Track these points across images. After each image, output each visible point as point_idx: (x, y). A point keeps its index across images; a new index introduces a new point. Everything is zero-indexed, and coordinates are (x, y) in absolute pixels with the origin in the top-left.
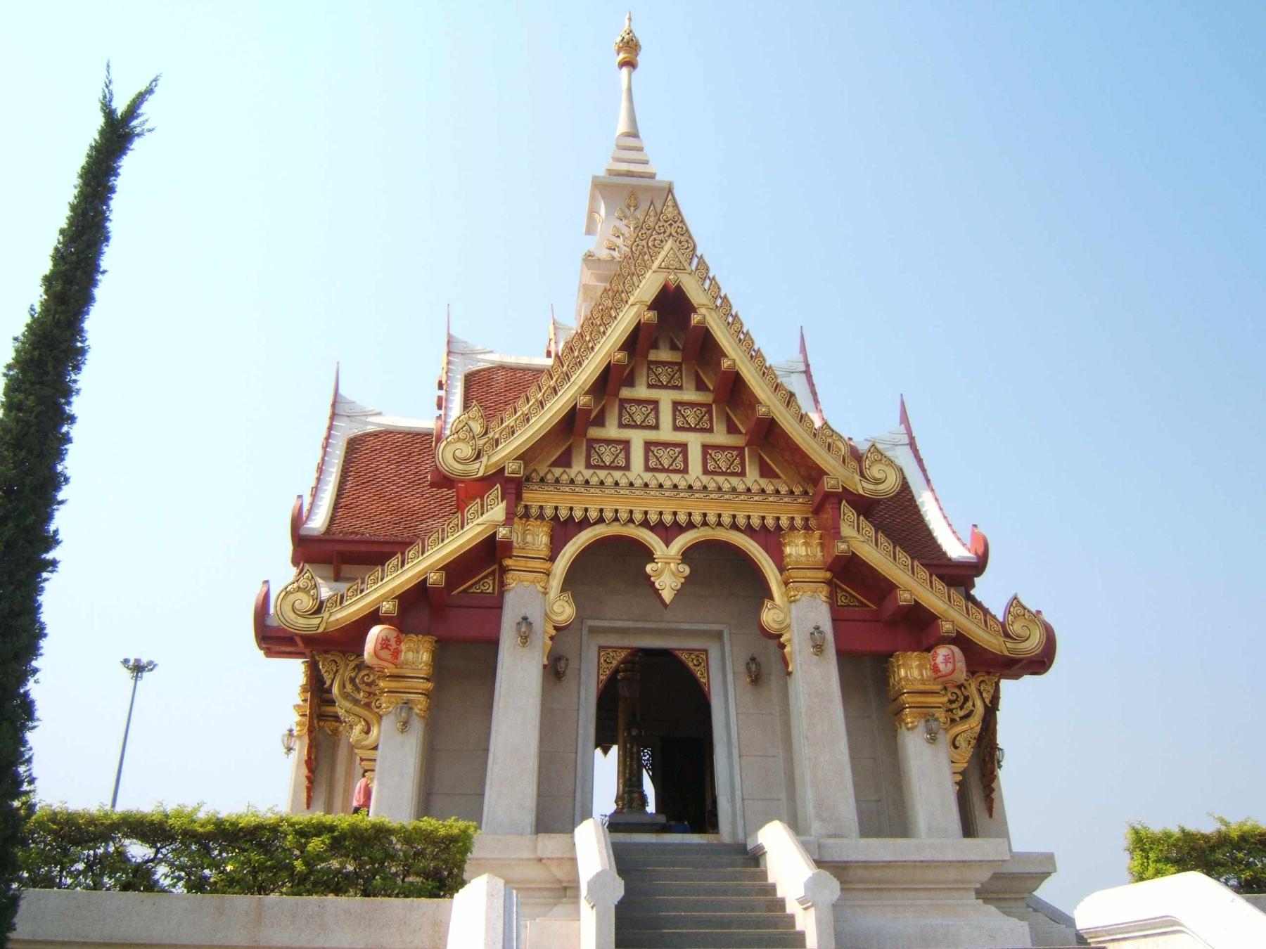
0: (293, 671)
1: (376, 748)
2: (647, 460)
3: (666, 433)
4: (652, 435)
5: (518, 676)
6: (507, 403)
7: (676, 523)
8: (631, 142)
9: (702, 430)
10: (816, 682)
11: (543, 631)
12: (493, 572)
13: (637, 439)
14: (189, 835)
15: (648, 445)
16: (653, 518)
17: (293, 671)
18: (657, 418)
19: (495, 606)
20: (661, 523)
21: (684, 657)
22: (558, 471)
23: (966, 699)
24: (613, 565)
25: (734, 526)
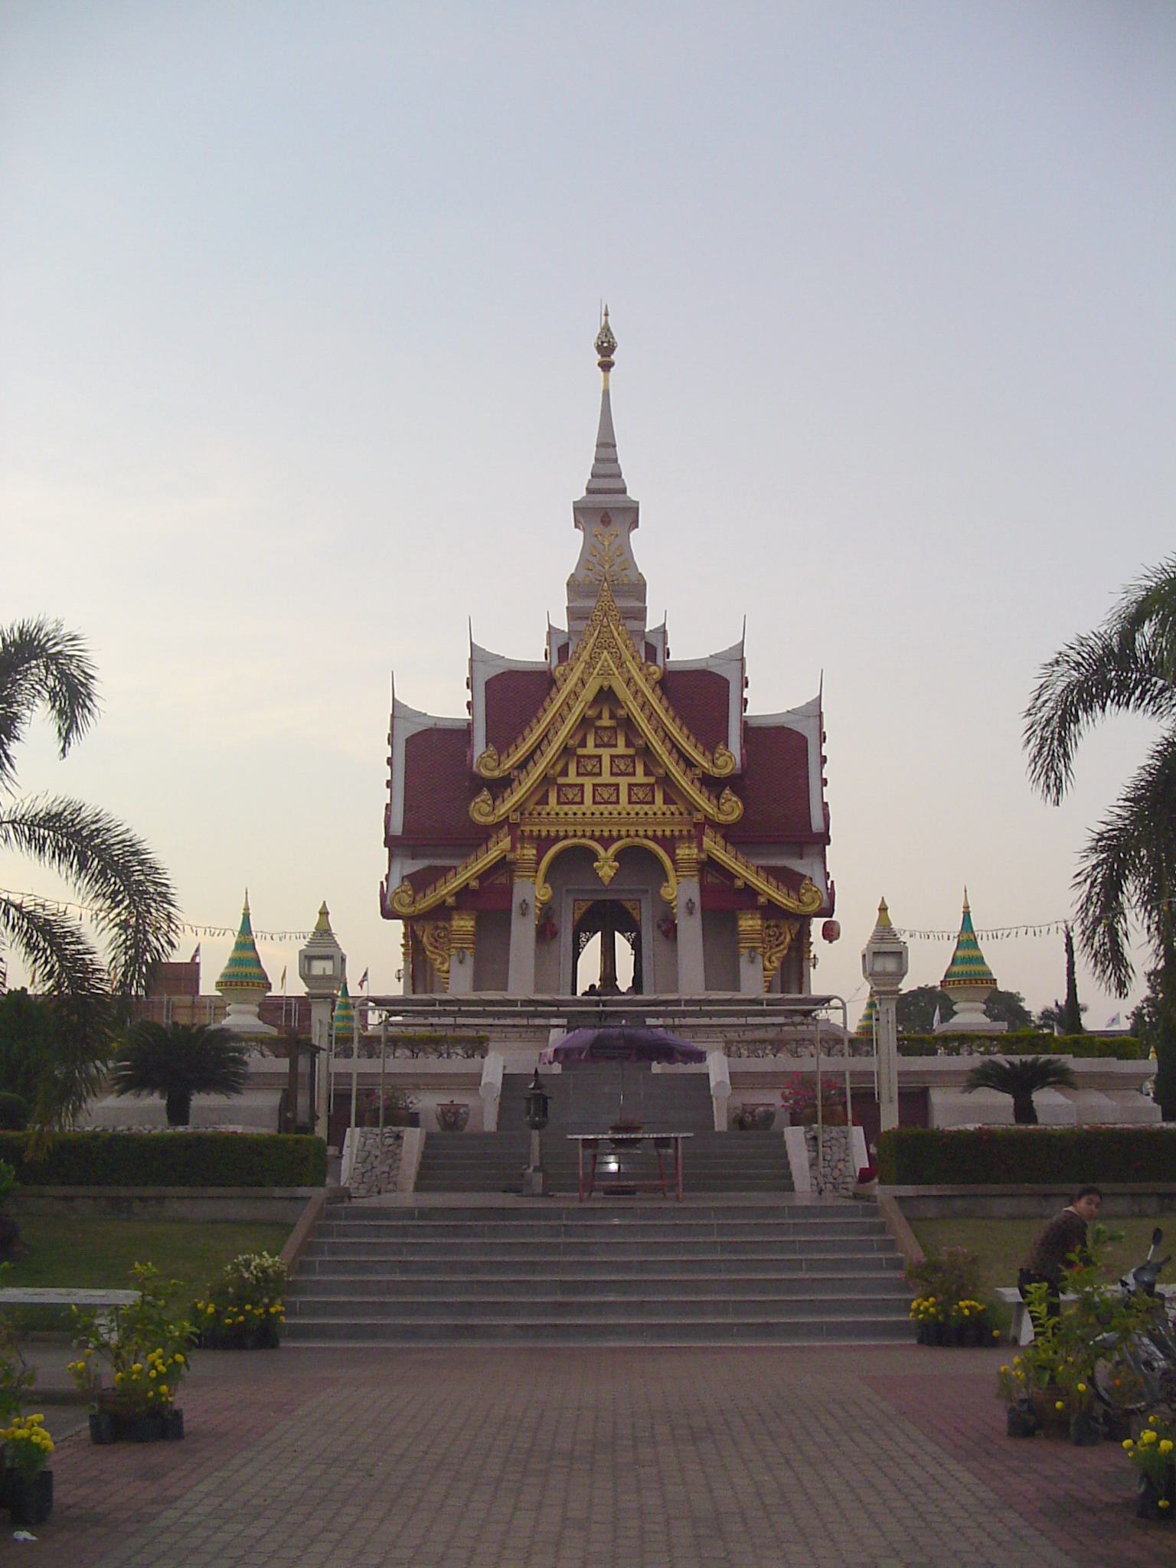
0: (398, 926)
3: (606, 778)
4: (598, 780)
7: (611, 836)
9: (628, 774)
10: (690, 929)
11: (534, 911)
13: (588, 782)
16: (597, 834)
17: (398, 926)
19: (508, 892)
22: (539, 808)
24: (578, 859)
25: (646, 837)
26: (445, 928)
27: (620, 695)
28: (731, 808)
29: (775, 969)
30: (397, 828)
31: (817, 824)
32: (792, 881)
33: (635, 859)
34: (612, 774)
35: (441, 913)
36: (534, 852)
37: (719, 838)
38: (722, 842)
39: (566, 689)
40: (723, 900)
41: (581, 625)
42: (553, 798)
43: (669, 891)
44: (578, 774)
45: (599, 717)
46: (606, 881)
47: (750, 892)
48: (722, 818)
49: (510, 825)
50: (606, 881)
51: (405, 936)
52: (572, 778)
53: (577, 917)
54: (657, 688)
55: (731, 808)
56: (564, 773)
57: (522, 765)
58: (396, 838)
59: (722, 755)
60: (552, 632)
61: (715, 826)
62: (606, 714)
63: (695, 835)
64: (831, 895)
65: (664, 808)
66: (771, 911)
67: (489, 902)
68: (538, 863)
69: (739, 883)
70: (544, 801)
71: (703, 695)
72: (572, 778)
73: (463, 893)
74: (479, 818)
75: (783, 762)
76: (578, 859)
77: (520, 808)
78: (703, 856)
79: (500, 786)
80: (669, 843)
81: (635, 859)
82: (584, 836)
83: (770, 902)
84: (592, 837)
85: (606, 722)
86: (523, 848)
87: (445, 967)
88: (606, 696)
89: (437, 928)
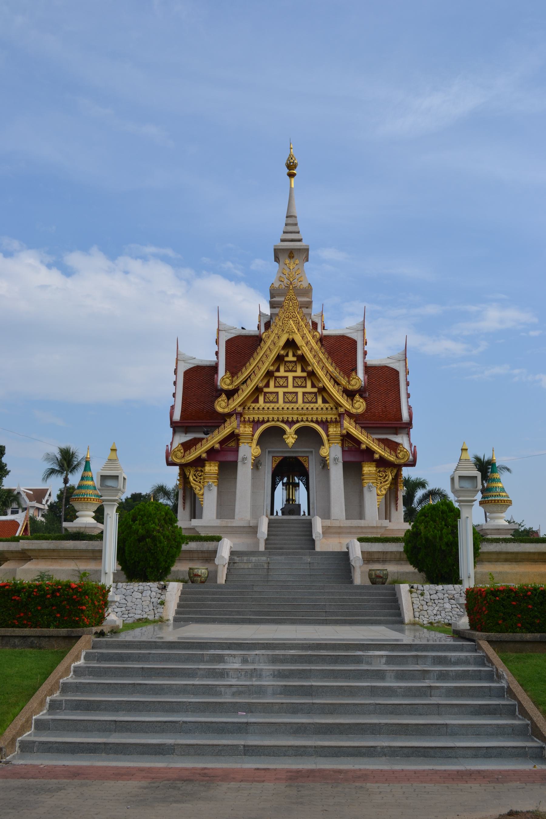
1: (203, 495)
2: (284, 399)
3: (290, 389)
4: (286, 390)
5: (244, 472)
6: (239, 371)
8: (290, 221)
10: (337, 473)
11: (250, 461)
12: (235, 440)
13: (281, 391)
14: (431, 757)
15: (285, 393)
17: (176, 470)
18: (287, 383)
19: (237, 450)
20: (287, 421)
21: (301, 459)
22: (253, 405)
23: (386, 476)
24: (273, 435)
25: (312, 421)
26: (202, 471)
27: (299, 344)
28: (359, 406)
29: (383, 495)
30: (177, 416)
31: (405, 416)
32: (394, 447)
33: (307, 435)
34: (294, 387)
35: (199, 463)
36: (251, 429)
37: (352, 421)
38: (354, 424)
39: (269, 342)
40: (356, 458)
41: (276, 311)
42: (261, 399)
43: (324, 451)
44: (275, 387)
45: (287, 355)
46: (290, 445)
47: (369, 452)
48: (353, 411)
49: (237, 414)
50: (290, 445)
51: (180, 475)
52: (272, 389)
53: (274, 466)
54: (319, 342)
55: (359, 406)
56: (267, 385)
57: (244, 382)
58: (176, 422)
59: (354, 378)
60: (261, 315)
61: (350, 415)
62: (290, 354)
63: (338, 422)
64: (415, 455)
65: (322, 405)
66: (382, 463)
67: (225, 457)
68: (253, 435)
69: (363, 446)
70: (256, 401)
71: (342, 350)
72: (272, 389)
73: (211, 452)
74: (219, 409)
75: (385, 383)
76: (273, 435)
77: (243, 404)
78: (344, 432)
79: (230, 394)
80: (325, 424)
81: (307, 435)
82: (278, 421)
83: (381, 457)
84: (283, 421)
85: (291, 358)
86: (245, 427)
87: (201, 493)
88: (291, 344)
89: (197, 471)
